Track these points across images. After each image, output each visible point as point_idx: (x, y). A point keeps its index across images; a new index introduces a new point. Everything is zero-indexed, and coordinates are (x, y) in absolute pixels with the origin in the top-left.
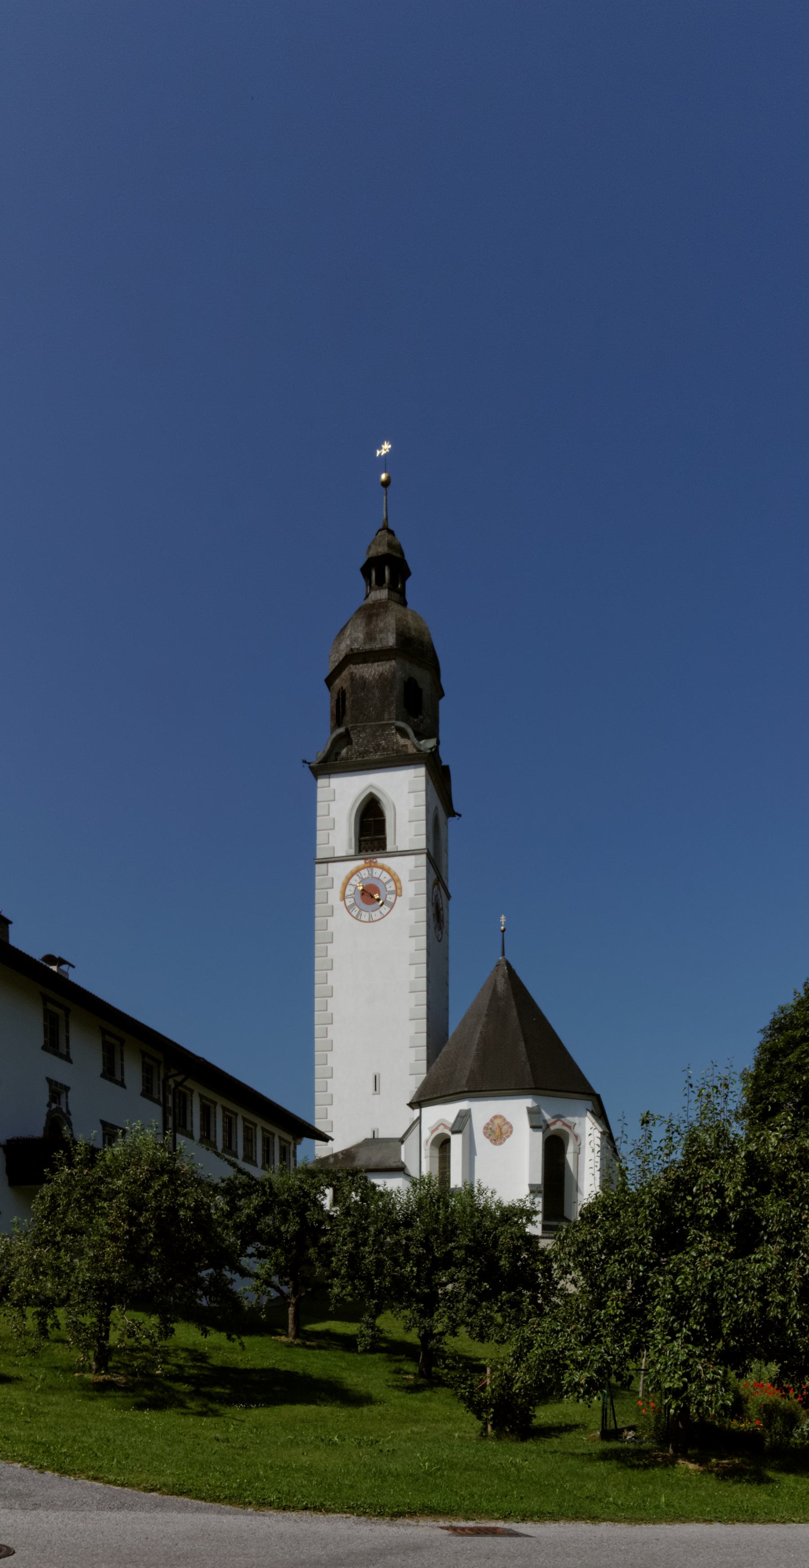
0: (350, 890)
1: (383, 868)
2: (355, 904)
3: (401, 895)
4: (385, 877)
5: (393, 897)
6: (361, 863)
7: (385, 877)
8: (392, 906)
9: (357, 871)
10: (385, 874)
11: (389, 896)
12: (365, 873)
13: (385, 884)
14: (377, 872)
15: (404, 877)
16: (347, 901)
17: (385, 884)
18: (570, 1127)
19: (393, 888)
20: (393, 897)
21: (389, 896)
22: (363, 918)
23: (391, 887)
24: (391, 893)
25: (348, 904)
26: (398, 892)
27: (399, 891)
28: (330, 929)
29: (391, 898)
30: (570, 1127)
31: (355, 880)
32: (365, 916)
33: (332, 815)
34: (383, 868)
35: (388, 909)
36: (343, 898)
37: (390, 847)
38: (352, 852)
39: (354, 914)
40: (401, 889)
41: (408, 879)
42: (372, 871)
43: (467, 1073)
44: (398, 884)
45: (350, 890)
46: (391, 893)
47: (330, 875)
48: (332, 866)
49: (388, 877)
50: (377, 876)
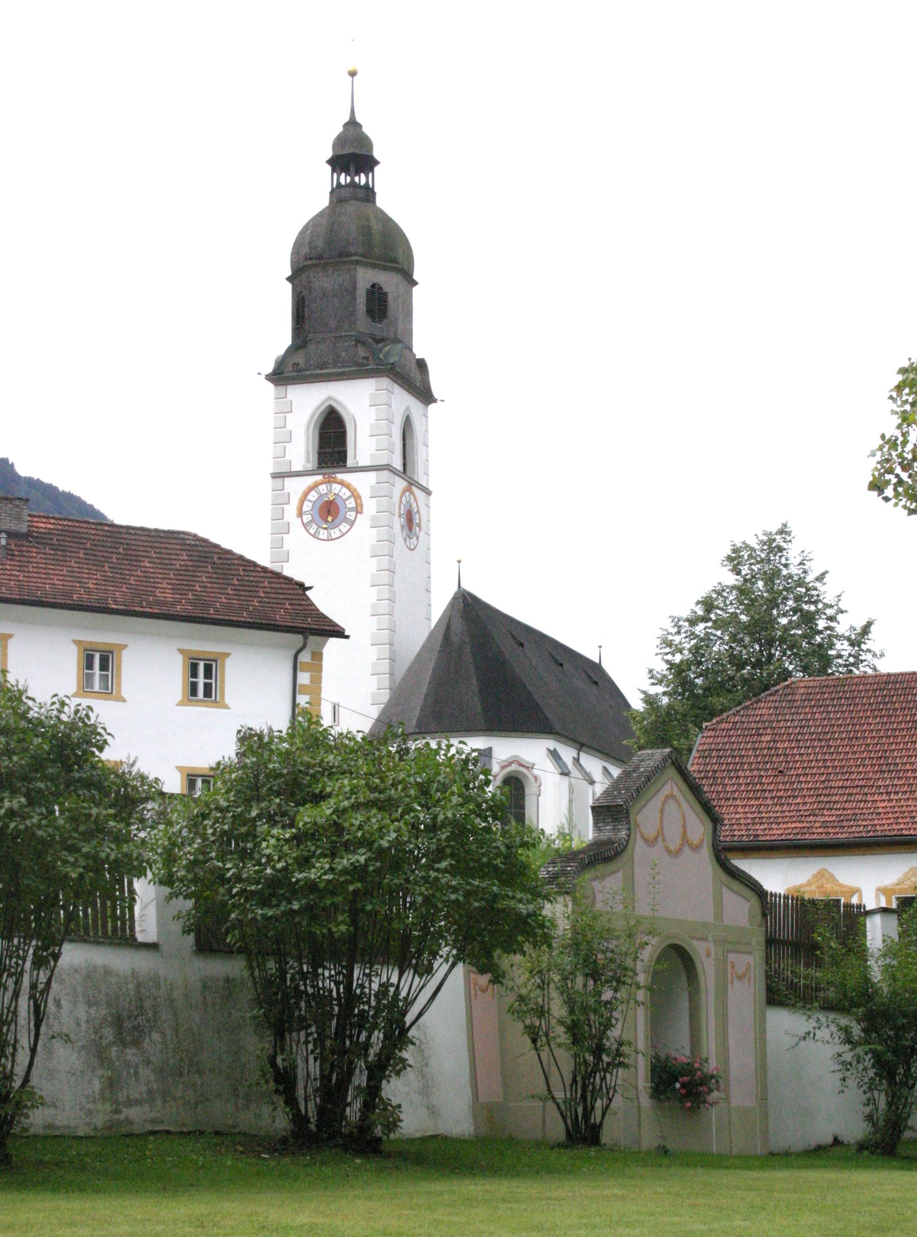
0: (307, 506)
1: (342, 483)
2: (312, 521)
3: (361, 513)
4: (345, 493)
5: (353, 514)
6: (320, 478)
7: (345, 493)
8: (352, 523)
9: (315, 486)
10: (345, 490)
11: (348, 513)
12: (323, 489)
13: (344, 501)
14: (336, 488)
15: (365, 493)
16: (304, 517)
17: (344, 501)
18: (527, 768)
19: (353, 505)
20: (353, 514)
21: (348, 513)
22: (321, 536)
23: (351, 503)
24: (351, 510)
25: (305, 521)
26: (358, 509)
27: (359, 508)
28: (286, 547)
29: (351, 515)
30: (527, 768)
31: (313, 496)
32: (323, 534)
33: (288, 427)
34: (342, 483)
35: (348, 527)
36: (300, 514)
37: (350, 462)
38: (312, 465)
39: (312, 531)
40: (362, 506)
41: (369, 495)
42: (331, 487)
43: (417, 712)
44: (359, 501)
45: (307, 506)
46: (351, 510)
47: (286, 490)
48: (288, 481)
49: (348, 493)
50: (336, 492)
